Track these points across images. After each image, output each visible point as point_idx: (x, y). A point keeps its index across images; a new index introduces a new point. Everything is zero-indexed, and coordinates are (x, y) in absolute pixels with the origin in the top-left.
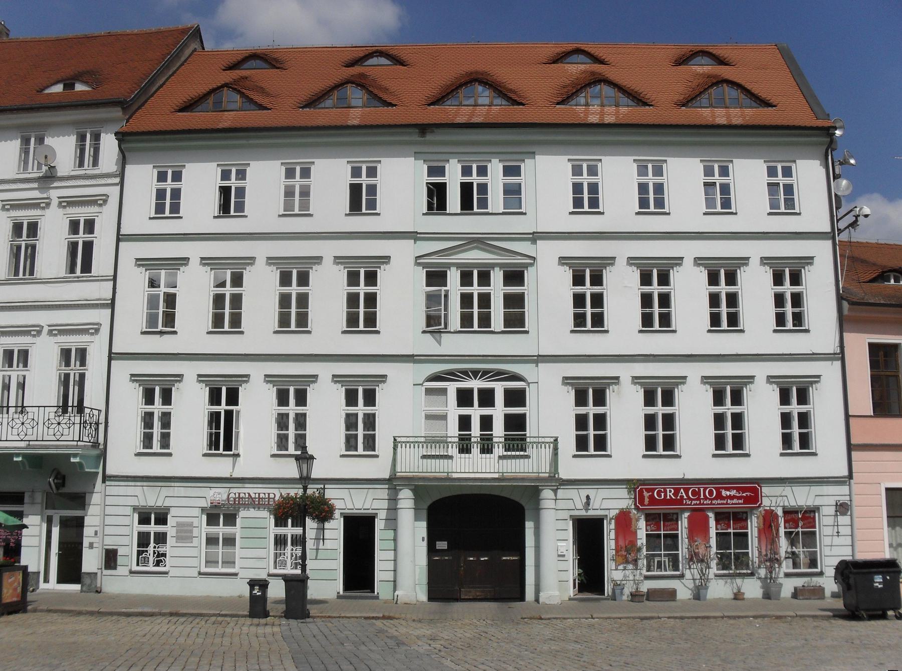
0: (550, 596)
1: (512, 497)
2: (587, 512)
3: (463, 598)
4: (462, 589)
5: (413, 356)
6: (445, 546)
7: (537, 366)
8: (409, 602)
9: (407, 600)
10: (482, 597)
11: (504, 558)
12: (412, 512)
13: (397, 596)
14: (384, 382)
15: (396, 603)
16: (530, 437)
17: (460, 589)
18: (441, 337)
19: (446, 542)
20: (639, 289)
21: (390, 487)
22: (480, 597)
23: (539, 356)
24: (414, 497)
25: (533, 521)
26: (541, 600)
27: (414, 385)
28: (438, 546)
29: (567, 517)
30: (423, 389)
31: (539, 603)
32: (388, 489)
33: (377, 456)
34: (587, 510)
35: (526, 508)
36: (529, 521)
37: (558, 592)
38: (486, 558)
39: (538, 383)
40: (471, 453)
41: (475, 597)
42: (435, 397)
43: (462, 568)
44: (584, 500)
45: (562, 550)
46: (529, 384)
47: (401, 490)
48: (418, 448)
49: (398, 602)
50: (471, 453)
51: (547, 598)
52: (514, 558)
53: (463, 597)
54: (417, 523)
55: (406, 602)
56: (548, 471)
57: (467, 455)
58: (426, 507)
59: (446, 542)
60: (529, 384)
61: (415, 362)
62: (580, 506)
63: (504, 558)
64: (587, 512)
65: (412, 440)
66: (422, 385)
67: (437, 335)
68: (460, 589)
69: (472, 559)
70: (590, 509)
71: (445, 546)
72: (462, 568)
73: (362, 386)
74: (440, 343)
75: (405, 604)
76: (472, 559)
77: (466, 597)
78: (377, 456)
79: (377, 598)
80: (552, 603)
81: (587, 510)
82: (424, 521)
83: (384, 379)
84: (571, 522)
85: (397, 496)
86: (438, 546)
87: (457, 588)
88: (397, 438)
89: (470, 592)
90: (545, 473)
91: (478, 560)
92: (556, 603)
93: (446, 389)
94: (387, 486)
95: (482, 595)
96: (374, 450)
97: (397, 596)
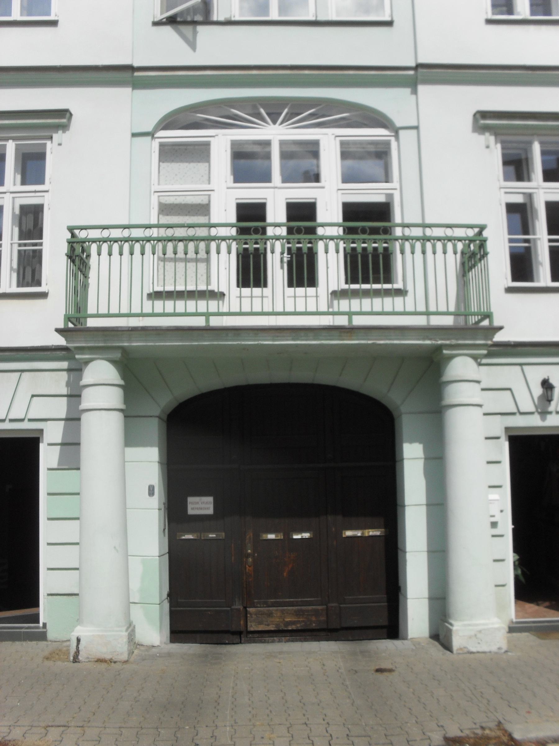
0: (480, 631)
1: (365, 390)
2: (543, 419)
3: (252, 629)
4: (248, 609)
5: (130, 68)
6: (208, 508)
7: (415, 92)
8: (108, 657)
9: (104, 652)
10: (299, 626)
11: (349, 533)
12: (116, 420)
13: (78, 640)
14: (65, 127)
15: (76, 659)
16: (404, 226)
17: (245, 608)
18: (195, 33)
19: (210, 499)
20: (501, 188)
21: (73, 367)
22: (294, 627)
23: (419, 66)
24: (122, 382)
25: (420, 443)
26: (457, 642)
27: (134, 135)
28: (192, 509)
29: (499, 431)
30: (155, 145)
31: (447, 646)
32: (69, 370)
33: (44, 295)
34: (544, 413)
35: (403, 409)
36: (411, 441)
37: (496, 620)
38: (306, 535)
39: (417, 128)
40: (265, 285)
41: (282, 627)
42: (186, 164)
43: (250, 560)
44: (538, 391)
45: (494, 510)
46: (396, 131)
47: (87, 362)
48: (132, 254)
49: (80, 658)
50: (265, 285)
51: (470, 637)
52: (371, 534)
53: (253, 627)
54: (134, 453)
55: (102, 656)
56: (452, 309)
57: (257, 291)
58: (157, 411)
59: (210, 499)
60: (396, 131)
61: (137, 85)
62: (527, 405)
63: (349, 533)
64: (543, 419)
65: (116, 233)
66: (151, 134)
67: (187, 30)
68: (245, 608)
69: (271, 536)
70: (550, 413)
71: (208, 508)
72: (250, 560)
73: (14, 139)
74: (193, 45)
75: (100, 661)
76: (271, 536)
77: (261, 628)
78: (44, 295)
79: (42, 636)
80: (484, 648)
81: (544, 413)
82: (152, 446)
83: (64, 121)
84: (506, 445)
85: (81, 380)
86: (192, 509)
87: (238, 606)
88: (77, 232)
89: (270, 615)
90: (447, 313)
91: (288, 537)
92: (494, 648)
93: (207, 145)
94: (65, 365)
95: (299, 622)
96: (39, 284)
97: (78, 640)
